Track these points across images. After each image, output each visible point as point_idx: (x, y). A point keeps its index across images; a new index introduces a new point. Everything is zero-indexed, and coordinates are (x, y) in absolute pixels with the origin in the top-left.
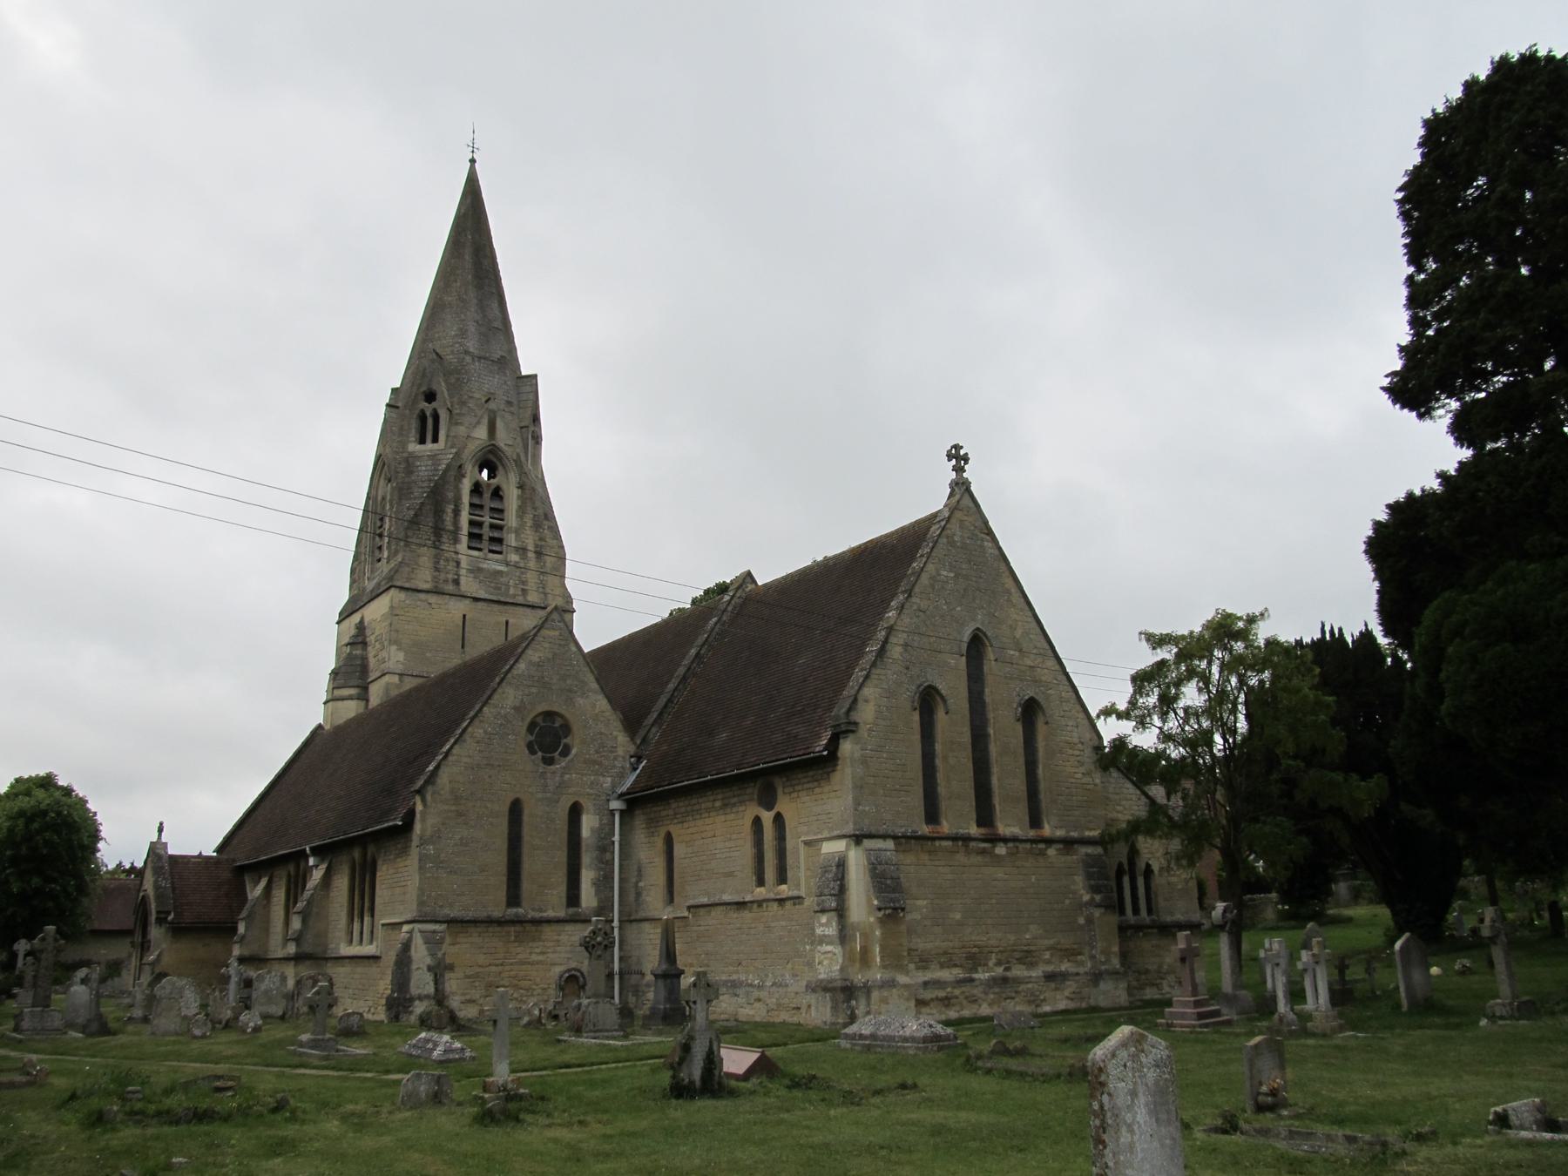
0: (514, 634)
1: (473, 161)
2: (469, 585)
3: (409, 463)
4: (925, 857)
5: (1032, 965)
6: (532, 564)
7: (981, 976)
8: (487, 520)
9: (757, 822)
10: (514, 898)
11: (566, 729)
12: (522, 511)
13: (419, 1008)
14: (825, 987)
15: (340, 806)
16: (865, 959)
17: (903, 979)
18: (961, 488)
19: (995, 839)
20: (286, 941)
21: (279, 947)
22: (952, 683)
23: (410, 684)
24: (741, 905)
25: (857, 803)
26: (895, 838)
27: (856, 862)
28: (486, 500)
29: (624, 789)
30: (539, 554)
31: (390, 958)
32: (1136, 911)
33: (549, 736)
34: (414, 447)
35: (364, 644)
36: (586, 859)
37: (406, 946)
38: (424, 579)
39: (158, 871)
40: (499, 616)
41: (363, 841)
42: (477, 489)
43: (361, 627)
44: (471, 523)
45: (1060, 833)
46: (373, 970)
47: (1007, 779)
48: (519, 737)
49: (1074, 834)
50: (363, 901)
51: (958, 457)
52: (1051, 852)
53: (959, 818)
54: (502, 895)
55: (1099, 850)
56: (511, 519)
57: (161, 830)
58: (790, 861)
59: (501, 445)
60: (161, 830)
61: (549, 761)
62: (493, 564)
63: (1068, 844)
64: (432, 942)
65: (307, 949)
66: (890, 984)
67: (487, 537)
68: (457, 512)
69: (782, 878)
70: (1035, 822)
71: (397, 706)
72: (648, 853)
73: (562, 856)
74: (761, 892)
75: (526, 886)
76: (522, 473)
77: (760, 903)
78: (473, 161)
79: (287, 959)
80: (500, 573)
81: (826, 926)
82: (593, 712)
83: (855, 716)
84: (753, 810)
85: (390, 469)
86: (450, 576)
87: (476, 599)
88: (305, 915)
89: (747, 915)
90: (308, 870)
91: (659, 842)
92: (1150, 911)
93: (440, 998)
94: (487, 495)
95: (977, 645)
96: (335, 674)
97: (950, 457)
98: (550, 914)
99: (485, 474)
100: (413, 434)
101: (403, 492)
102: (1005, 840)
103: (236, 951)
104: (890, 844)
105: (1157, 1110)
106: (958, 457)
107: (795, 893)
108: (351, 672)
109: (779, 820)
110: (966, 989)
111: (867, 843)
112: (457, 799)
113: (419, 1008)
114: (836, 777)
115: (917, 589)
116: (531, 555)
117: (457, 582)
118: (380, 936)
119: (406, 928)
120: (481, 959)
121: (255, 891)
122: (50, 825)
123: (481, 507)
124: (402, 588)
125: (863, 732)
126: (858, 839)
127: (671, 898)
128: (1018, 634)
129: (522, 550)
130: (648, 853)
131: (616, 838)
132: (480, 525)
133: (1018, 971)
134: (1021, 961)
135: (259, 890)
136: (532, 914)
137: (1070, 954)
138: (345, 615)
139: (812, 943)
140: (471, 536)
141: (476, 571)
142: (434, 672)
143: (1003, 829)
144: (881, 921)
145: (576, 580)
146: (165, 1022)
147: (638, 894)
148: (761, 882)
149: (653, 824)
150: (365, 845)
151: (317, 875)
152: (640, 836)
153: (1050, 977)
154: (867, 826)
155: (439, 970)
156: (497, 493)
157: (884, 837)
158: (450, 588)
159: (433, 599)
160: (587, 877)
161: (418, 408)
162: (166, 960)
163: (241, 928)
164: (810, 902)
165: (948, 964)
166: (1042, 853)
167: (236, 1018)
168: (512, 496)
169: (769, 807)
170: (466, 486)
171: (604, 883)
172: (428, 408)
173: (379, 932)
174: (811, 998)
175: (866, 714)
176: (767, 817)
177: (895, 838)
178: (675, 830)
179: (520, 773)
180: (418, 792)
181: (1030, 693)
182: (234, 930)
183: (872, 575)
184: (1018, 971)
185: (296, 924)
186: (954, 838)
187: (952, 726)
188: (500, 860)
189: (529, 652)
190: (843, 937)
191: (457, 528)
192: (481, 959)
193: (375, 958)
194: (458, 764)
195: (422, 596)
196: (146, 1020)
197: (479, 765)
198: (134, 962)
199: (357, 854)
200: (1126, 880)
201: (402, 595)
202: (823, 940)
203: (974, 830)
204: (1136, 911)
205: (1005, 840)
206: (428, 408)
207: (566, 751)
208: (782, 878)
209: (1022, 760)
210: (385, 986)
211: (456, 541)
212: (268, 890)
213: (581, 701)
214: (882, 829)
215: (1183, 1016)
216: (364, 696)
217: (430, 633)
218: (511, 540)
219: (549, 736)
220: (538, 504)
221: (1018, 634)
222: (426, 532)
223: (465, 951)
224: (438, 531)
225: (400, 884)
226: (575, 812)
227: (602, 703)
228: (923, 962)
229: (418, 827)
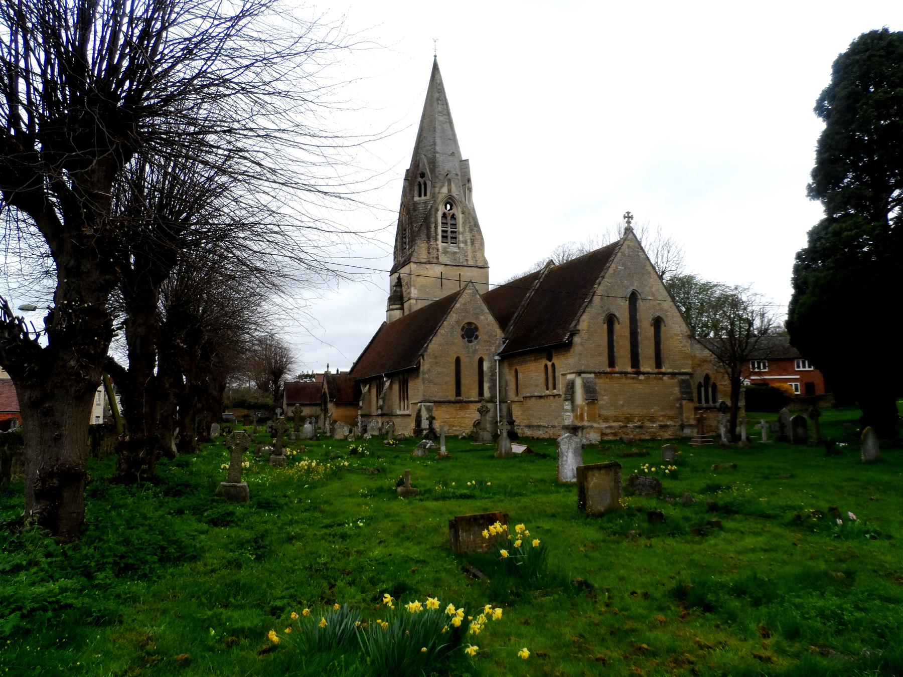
1: (435, 56)
2: (443, 259)
3: (415, 204)
4: (608, 380)
5: (654, 422)
6: (469, 247)
7: (630, 425)
8: (449, 229)
9: (546, 366)
10: (458, 393)
11: (476, 329)
12: (464, 224)
13: (425, 432)
16: (581, 418)
17: (595, 425)
18: (629, 230)
19: (639, 373)
20: (378, 408)
22: (622, 310)
24: (541, 397)
26: (594, 373)
27: (578, 382)
28: (450, 222)
29: (499, 351)
30: (472, 243)
31: (414, 416)
32: (707, 401)
33: (470, 332)
34: (416, 199)
36: (486, 379)
37: (420, 410)
39: (328, 383)
41: (404, 372)
42: (444, 216)
43: (399, 279)
44: (443, 231)
45: (669, 370)
46: (408, 420)
47: (647, 349)
48: (458, 332)
49: (676, 371)
50: (404, 395)
51: (629, 217)
52: (665, 378)
53: (622, 364)
54: (454, 392)
61: (470, 342)
62: (452, 248)
63: (673, 375)
64: (429, 410)
65: (385, 412)
67: (451, 237)
68: (436, 227)
69: (554, 388)
73: (476, 378)
74: (547, 392)
75: (463, 389)
78: (435, 56)
79: (378, 415)
80: (455, 253)
82: (487, 321)
83: (579, 327)
84: (545, 362)
86: (435, 255)
88: (384, 399)
89: (543, 401)
90: (384, 383)
91: (513, 372)
94: (449, 218)
95: (633, 298)
96: (390, 299)
97: (625, 217)
98: (472, 399)
99: (448, 207)
100: (416, 193)
102: (643, 373)
103: (359, 412)
104: (592, 375)
105: (575, 453)
108: (397, 298)
109: (553, 365)
110: (624, 430)
111: (583, 375)
112: (436, 357)
113: (425, 432)
116: (469, 243)
117: (437, 258)
120: (447, 416)
121: (365, 390)
126: (579, 373)
127: (517, 395)
128: (654, 290)
129: (465, 242)
130: (509, 377)
132: (446, 232)
134: (649, 420)
136: (465, 400)
137: (671, 418)
138: (393, 272)
140: (443, 237)
143: (642, 369)
144: (588, 404)
145: (490, 253)
147: (506, 392)
148: (547, 389)
149: (511, 365)
151: (387, 384)
153: (661, 427)
154: (583, 368)
155: (431, 419)
157: (590, 373)
158: (435, 260)
159: (428, 266)
160: (486, 386)
161: (418, 179)
162: (334, 415)
163: (361, 404)
164: (563, 396)
165: (617, 420)
166: (661, 379)
169: (550, 361)
170: (440, 214)
171: (492, 388)
172: (422, 180)
173: (410, 406)
176: (549, 364)
177: (594, 373)
178: (518, 368)
179: (459, 347)
181: (658, 314)
183: (595, 263)
184: (648, 424)
185: (381, 403)
186: (621, 373)
187: (622, 330)
188: (452, 380)
190: (573, 410)
191: (437, 235)
192: (447, 416)
193: (409, 415)
194: (435, 345)
197: (444, 342)
198: (322, 416)
200: (703, 389)
202: (567, 411)
203: (629, 370)
205: (643, 373)
206: (422, 180)
207: (477, 337)
208: (554, 388)
209: (653, 341)
210: (413, 425)
211: (436, 240)
212: (370, 388)
214: (589, 370)
215: (697, 442)
216: (402, 309)
218: (461, 238)
219: (470, 332)
220: (471, 220)
221: (654, 290)
222: (423, 235)
223: (441, 414)
224: (428, 237)
225: (417, 389)
226: (481, 361)
227: (491, 318)
228: (606, 420)
229: (421, 368)
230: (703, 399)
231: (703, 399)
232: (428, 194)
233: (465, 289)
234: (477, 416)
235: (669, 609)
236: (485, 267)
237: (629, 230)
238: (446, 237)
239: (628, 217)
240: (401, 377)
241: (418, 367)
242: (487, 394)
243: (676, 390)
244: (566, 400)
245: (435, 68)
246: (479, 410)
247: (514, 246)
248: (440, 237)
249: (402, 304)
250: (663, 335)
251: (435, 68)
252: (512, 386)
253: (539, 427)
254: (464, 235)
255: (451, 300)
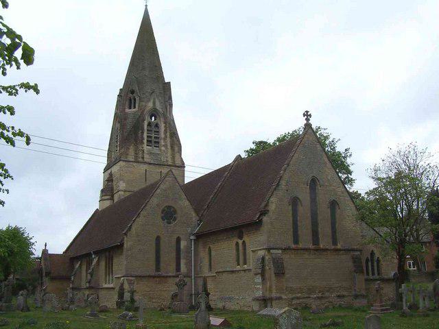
0: (151, 180)
1: (146, 6)
2: (147, 158)
3: (126, 114)
8: (153, 135)
9: (237, 244)
10: (158, 269)
11: (175, 212)
12: (166, 131)
14: (257, 299)
15: (101, 238)
18: (308, 126)
21: (84, 284)
22: (304, 196)
23: (128, 194)
25: (268, 237)
31: (117, 288)
32: (373, 274)
33: (169, 214)
34: (127, 110)
35: (112, 181)
36: (182, 255)
37: (122, 285)
38: (131, 158)
40: (158, 169)
42: (149, 124)
43: (111, 175)
46: (112, 292)
51: (307, 115)
53: (306, 241)
55: (359, 253)
56: (162, 135)
57: (46, 245)
58: (247, 257)
59: (158, 108)
60: (46, 245)
61: (169, 223)
62: (156, 150)
63: (348, 251)
64: (130, 283)
66: (280, 298)
68: (143, 133)
69: (245, 263)
70: (335, 243)
71: (123, 201)
72: (203, 254)
73: (174, 254)
74: (238, 268)
75: (162, 264)
76: (165, 118)
77: (238, 271)
78: (146, 6)
79: (87, 288)
81: (258, 279)
82: (184, 204)
84: (236, 240)
85: (119, 118)
87: (150, 164)
90: (92, 260)
92: (378, 274)
93: (132, 301)
95: (314, 183)
97: (304, 115)
99: (153, 118)
101: (123, 127)
103: (71, 286)
104: (280, 251)
106: (307, 115)
107: (249, 268)
108: (108, 190)
114: (262, 229)
115: (291, 163)
117: (143, 158)
118: (113, 280)
119: (122, 279)
122: (15, 240)
123: (151, 131)
124: (123, 161)
125: (270, 214)
129: (166, 146)
131: (193, 249)
132: (151, 137)
133: (327, 294)
134: (328, 291)
135: (77, 266)
136: (164, 274)
138: (106, 170)
139: (124, 302)
141: (150, 153)
142: (136, 189)
145: (187, 155)
146: (48, 307)
148: (239, 265)
150: (111, 252)
151: (95, 261)
152: (201, 249)
155: (132, 292)
156: (157, 125)
159: (135, 164)
161: (128, 97)
167: (68, 307)
168: (162, 126)
170: (146, 123)
174: (253, 303)
175: (272, 207)
176: (240, 242)
180: (125, 234)
182: (70, 279)
183: (287, 147)
184: (327, 294)
185: (89, 277)
189: (162, 186)
191: (143, 139)
195: (131, 163)
196: (41, 307)
199: (107, 254)
200: (370, 264)
201: (124, 163)
203: (311, 246)
204: (373, 274)
210: (116, 297)
211: (143, 143)
213: (180, 202)
216: (112, 198)
217: (134, 176)
218: (162, 143)
219: (169, 214)
223: (142, 288)
225: (121, 265)
226: (178, 240)
227: (187, 203)
229: (125, 246)
230: (376, 271)
231: (376, 271)
232: (137, 105)
233: (165, 177)
234: (174, 289)
235: (13, 133)
236: (182, 166)
237: (308, 126)
238: (151, 141)
239: (307, 115)
240: (107, 254)
241: (122, 245)
242: (183, 268)
243: (351, 264)
244: (256, 274)
245: (146, 30)
246: (177, 284)
247: (208, 141)
248: (145, 141)
249: (113, 196)
250: (337, 216)
251: (146, 30)
252: (206, 261)
253: (230, 299)
254: (165, 142)
255: (154, 187)
